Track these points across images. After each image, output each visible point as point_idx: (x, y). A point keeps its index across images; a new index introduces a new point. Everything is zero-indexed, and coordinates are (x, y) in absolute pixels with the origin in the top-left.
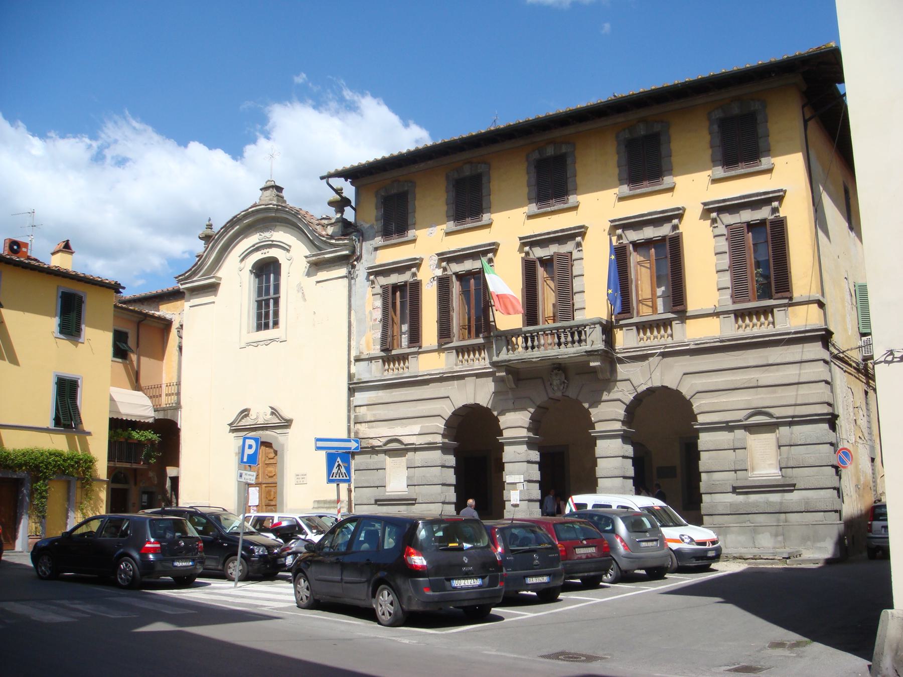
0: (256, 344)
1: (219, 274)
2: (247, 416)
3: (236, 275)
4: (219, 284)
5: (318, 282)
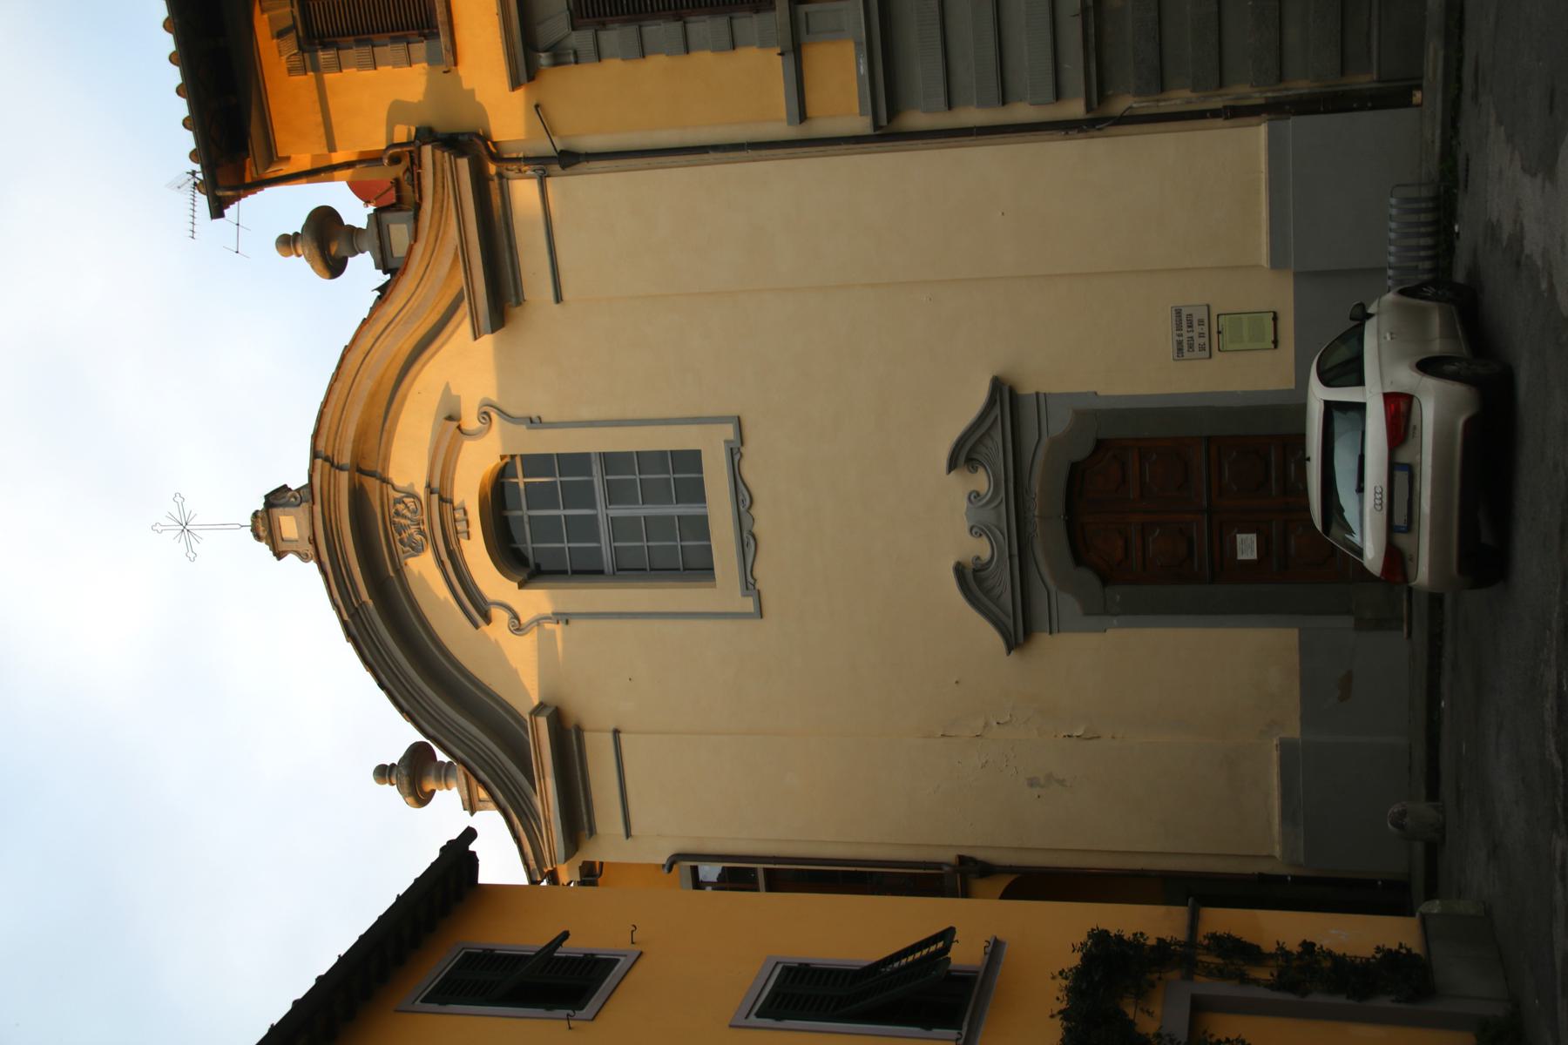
5: (1275, 319)
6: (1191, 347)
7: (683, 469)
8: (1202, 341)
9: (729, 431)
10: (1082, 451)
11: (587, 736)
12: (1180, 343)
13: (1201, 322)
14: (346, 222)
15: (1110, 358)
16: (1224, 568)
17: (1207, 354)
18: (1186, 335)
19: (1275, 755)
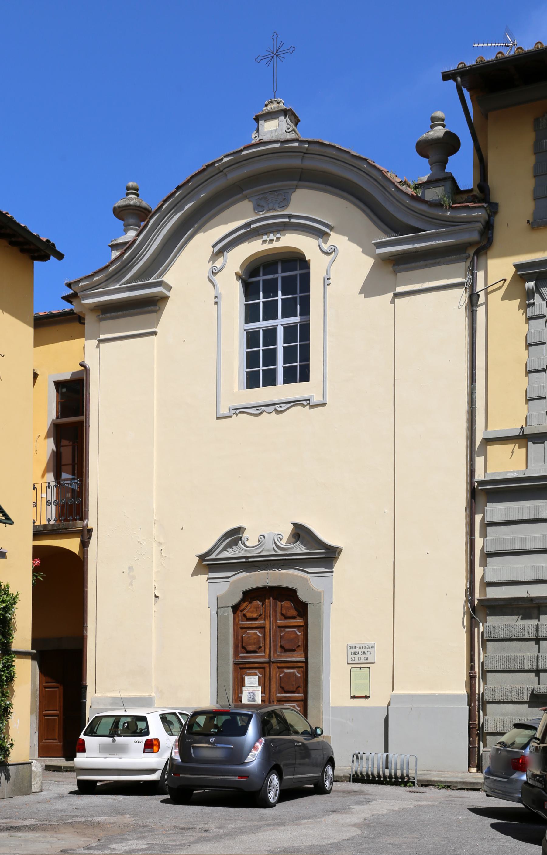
0: (257, 410)
1: (166, 278)
2: (235, 543)
3: (203, 281)
4: (165, 298)
5: (367, 697)
6: (354, 653)
7: (299, 372)
8: (357, 659)
9: (317, 399)
10: (302, 596)
11: (154, 314)
12: (356, 648)
13: (366, 659)
14: (450, 158)
15: (345, 612)
16: (241, 669)
17: (350, 661)
18: (360, 651)
19: (146, 694)
